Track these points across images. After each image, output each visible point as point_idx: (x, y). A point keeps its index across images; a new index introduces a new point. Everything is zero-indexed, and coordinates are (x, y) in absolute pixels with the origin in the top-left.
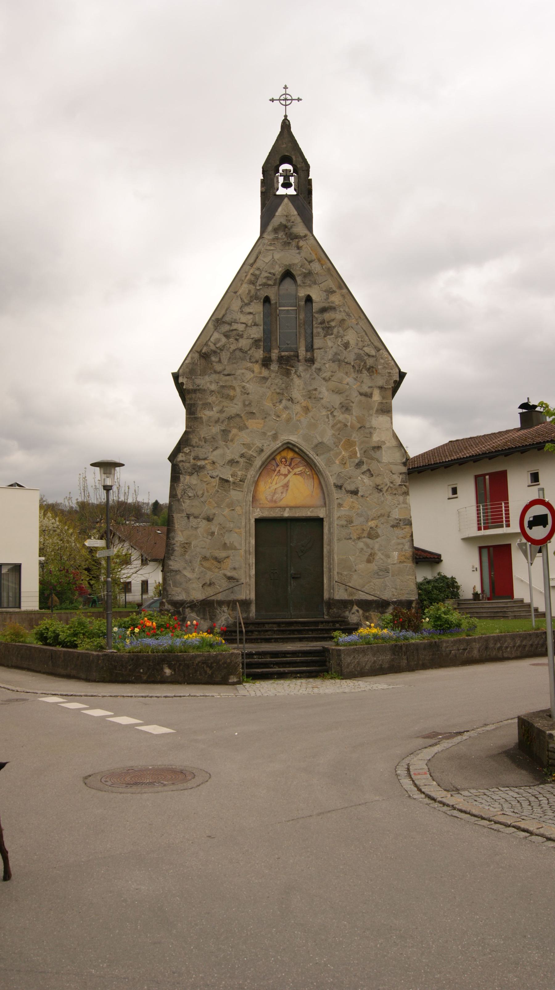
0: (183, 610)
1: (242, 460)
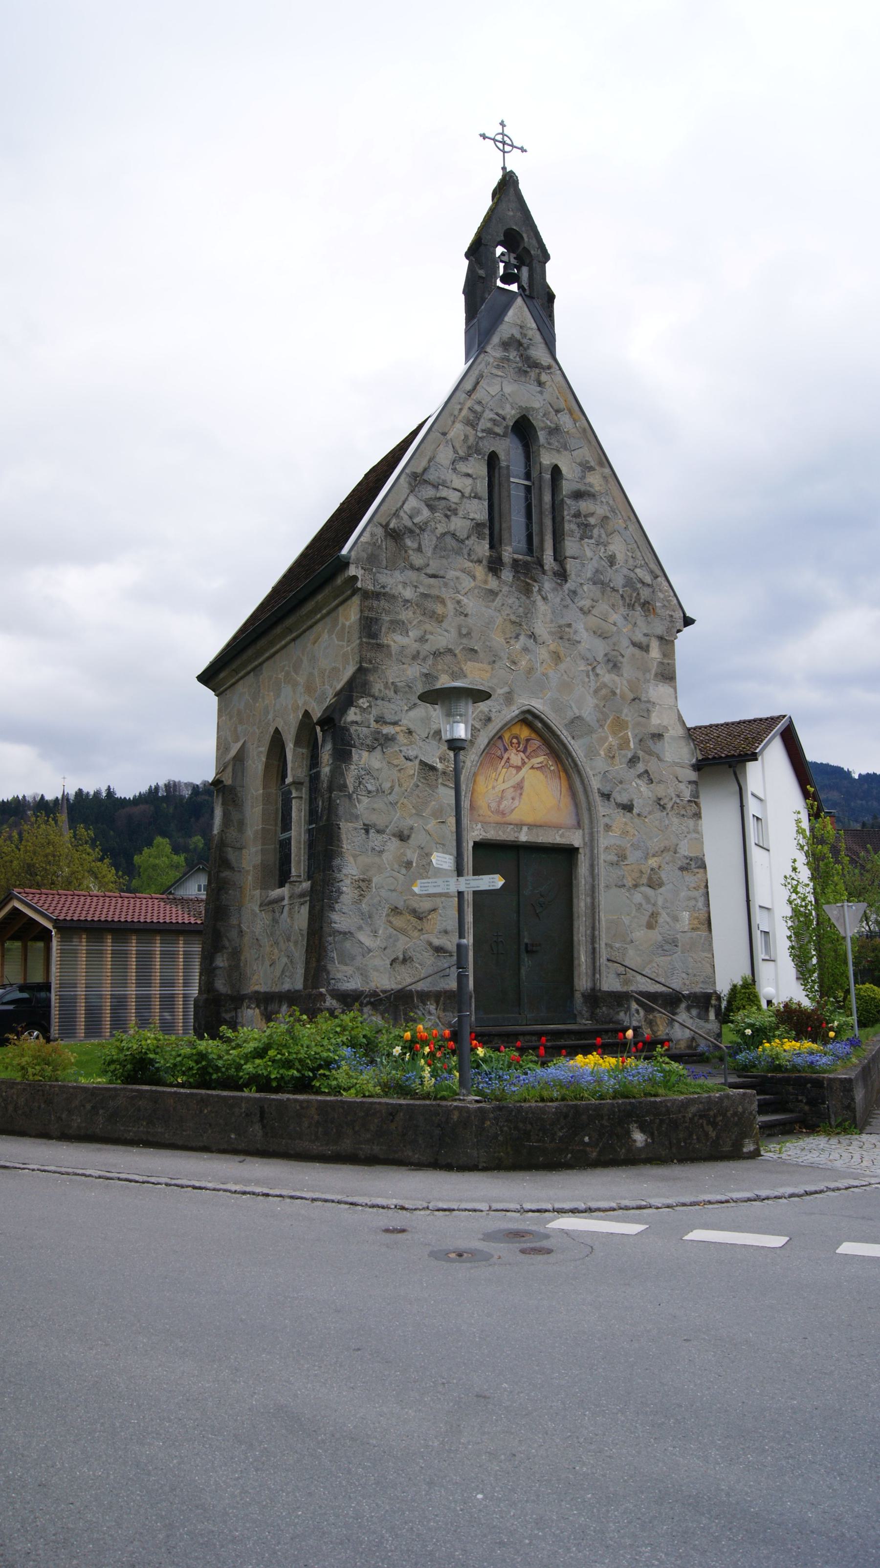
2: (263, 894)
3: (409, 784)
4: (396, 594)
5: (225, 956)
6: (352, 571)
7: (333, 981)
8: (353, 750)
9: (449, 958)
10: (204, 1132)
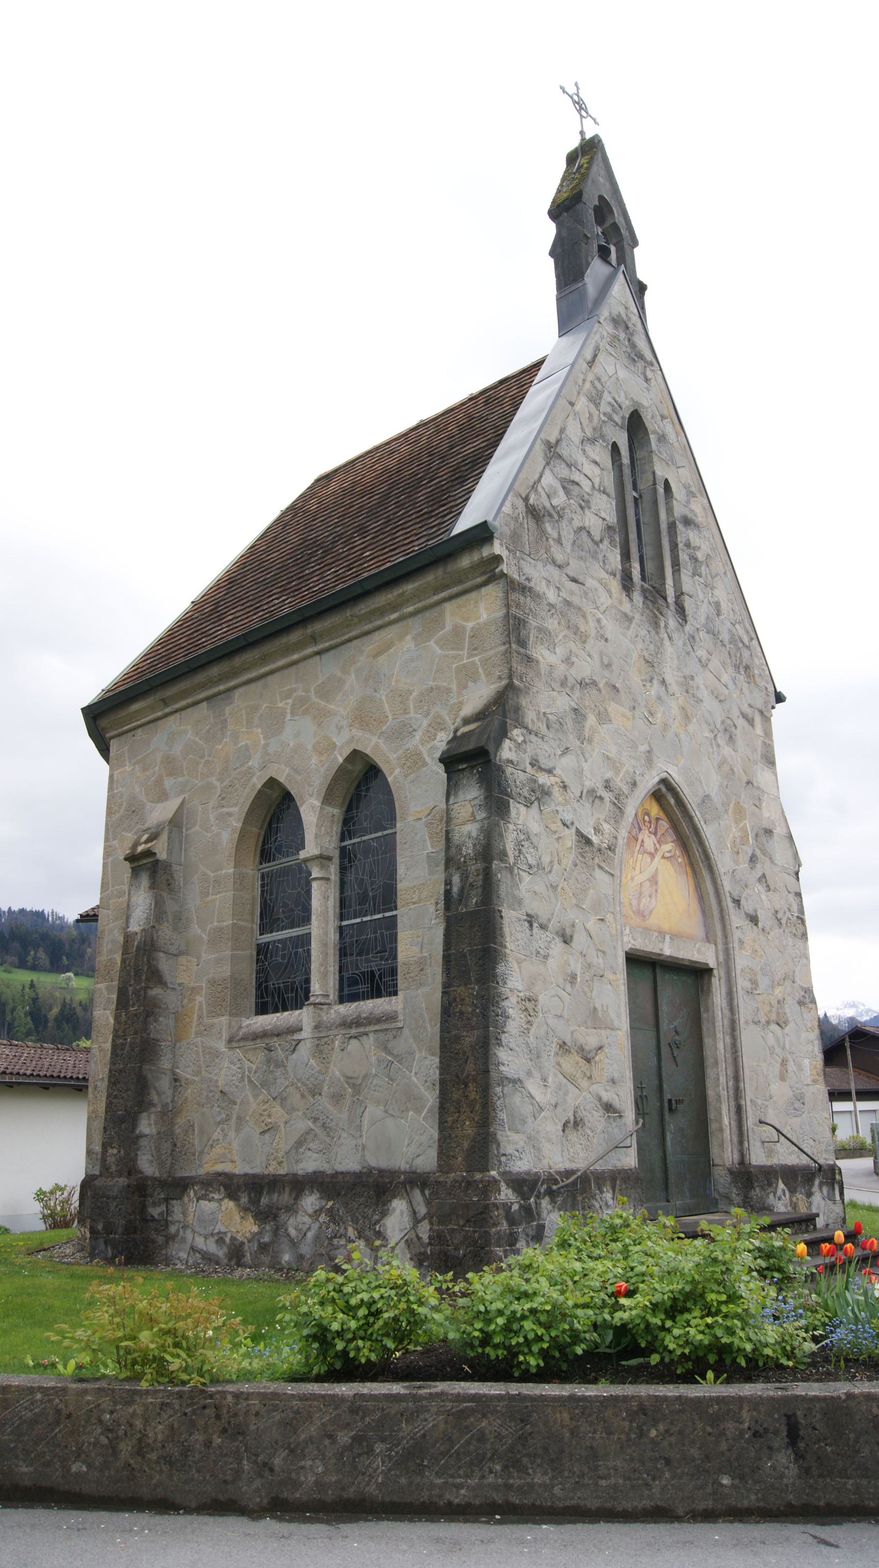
0: (536, 1203)
1: (606, 795)
2: (233, 1023)
3: (568, 862)
4: (541, 593)
5: (153, 1117)
6: (497, 548)
7: (503, 1159)
8: (511, 801)
9: (618, 1120)
10: (654, 1479)
